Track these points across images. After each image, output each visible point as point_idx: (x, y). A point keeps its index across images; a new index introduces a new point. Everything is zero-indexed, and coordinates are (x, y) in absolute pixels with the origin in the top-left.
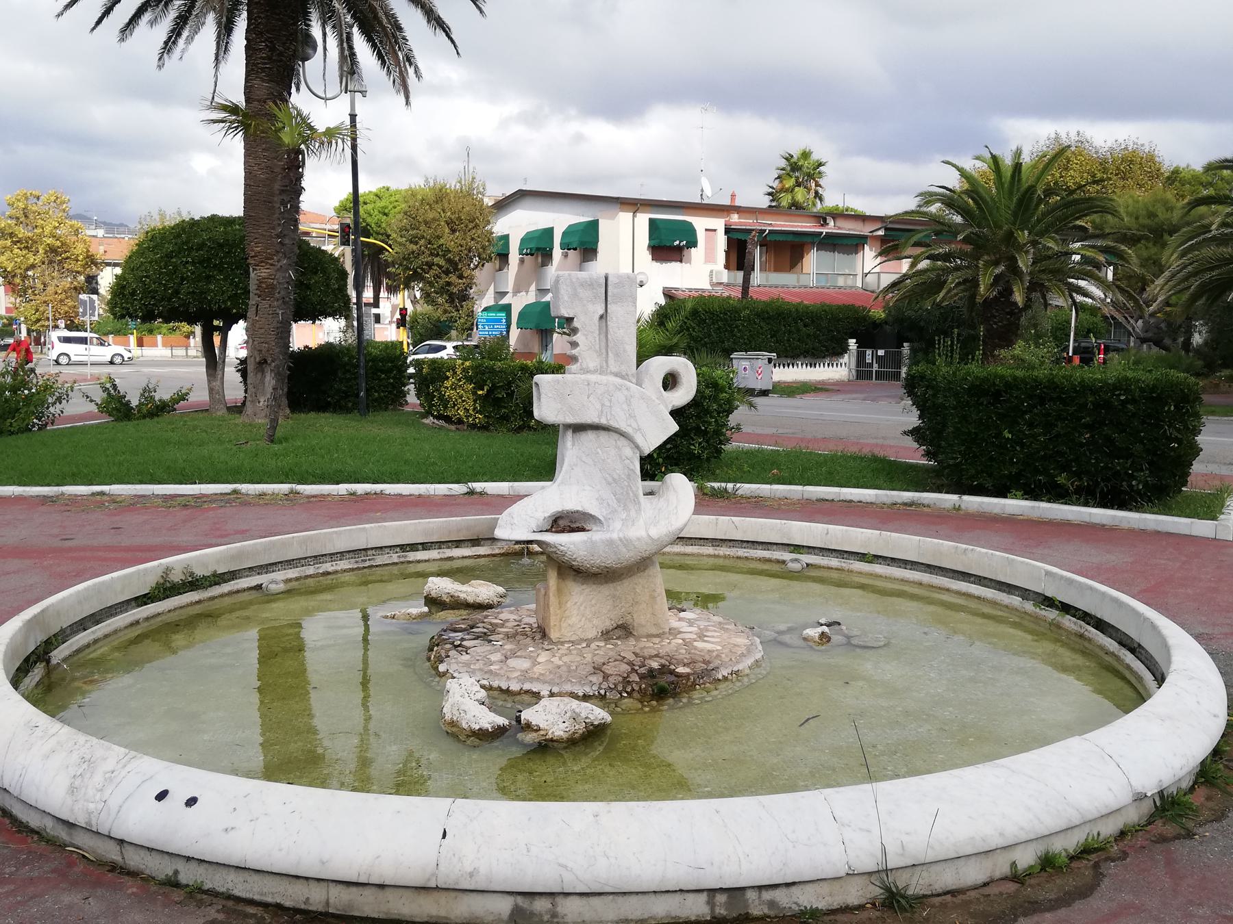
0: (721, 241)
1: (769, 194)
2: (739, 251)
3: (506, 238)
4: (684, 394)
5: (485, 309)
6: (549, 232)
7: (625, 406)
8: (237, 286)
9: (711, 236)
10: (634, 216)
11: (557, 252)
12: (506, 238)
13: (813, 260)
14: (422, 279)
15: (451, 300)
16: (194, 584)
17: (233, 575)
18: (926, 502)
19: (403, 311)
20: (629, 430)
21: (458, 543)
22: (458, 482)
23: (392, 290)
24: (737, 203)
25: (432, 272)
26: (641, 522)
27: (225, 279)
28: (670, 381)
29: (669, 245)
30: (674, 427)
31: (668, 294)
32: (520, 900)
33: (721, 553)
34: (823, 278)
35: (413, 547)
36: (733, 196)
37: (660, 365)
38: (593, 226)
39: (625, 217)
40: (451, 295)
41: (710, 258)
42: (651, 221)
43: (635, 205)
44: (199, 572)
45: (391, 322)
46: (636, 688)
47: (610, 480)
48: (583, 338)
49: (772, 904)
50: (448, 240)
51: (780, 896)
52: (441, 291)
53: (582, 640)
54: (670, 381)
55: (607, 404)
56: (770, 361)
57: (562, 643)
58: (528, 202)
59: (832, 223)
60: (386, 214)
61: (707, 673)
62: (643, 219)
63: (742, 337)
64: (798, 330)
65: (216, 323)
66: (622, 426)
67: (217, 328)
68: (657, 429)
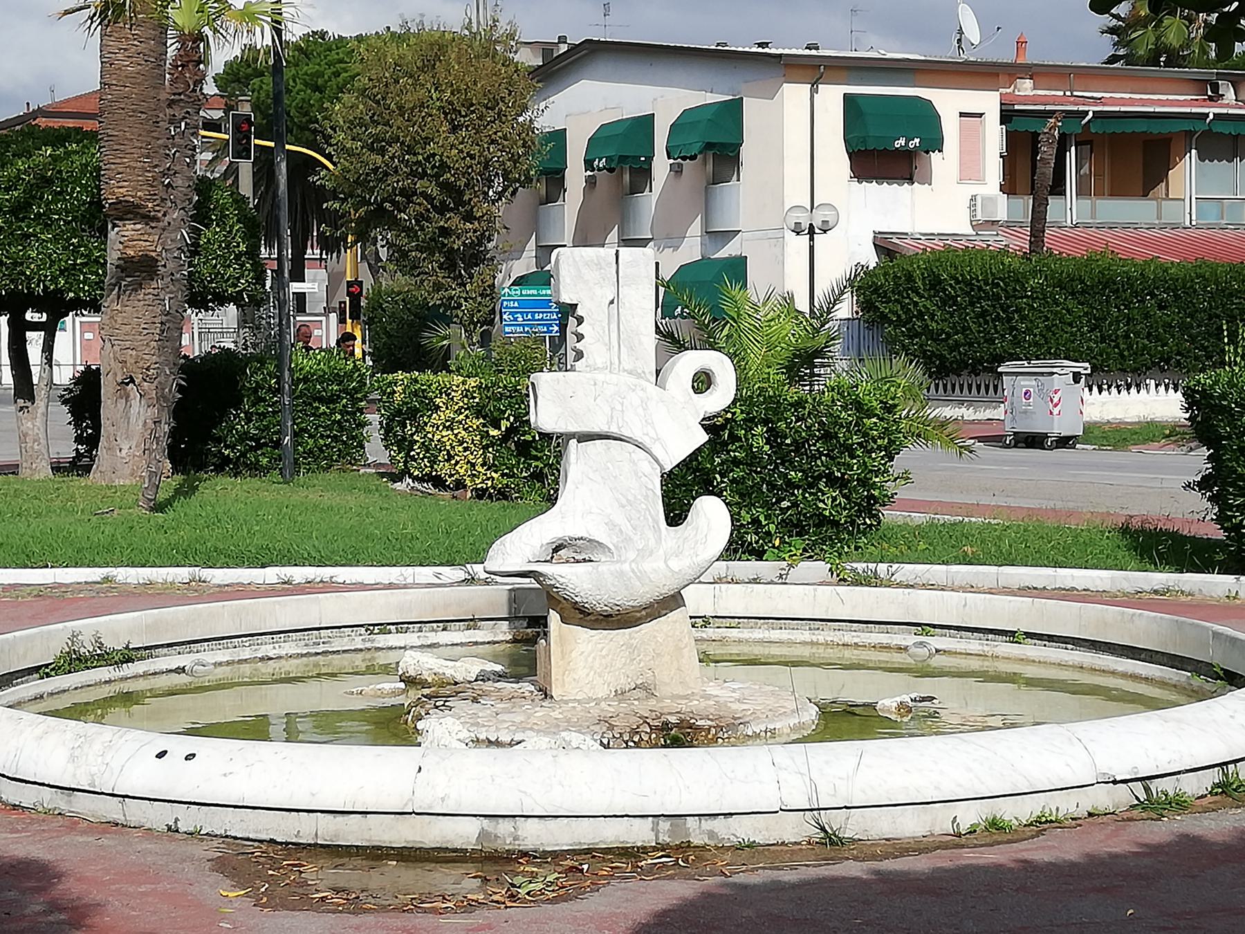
0: (994, 136)
1: (1112, 31)
2: (1030, 159)
3: (559, 137)
4: (720, 397)
5: (519, 282)
6: (647, 123)
7: (640, 410)
8: (75, 251)
9: (970, 125)
10: (814, 91)
11: (661, 166)
12: (559, 137)
13: (1187, 174)
14: (394, 223)
15: (450, 265)
16: (104, 658)
17: (149, 651)
18: (1186, 588)
19: (354, 289)
20: (647, 442)
21: (445, 624)
22: (450, 563)
23: (331, 245)
24: (1030, 58)
25: (411, 209)
26: (661, 552)
27: (55, 240)
28: (703, 382)
29: (886, 149)
30: (703, 437)
31: (884, 246)
32: (486, 821)
33: (821, 639)
34: (1212, 208)
35: (383, 628)
36: (1020, 43)
37: (691, 361)
38: (733, 110)
39: (795, 94)
40: (451, 254)
41: (969, 171)
42: (847, 98)
43: (814, 70)
44: (109, 644)
45: (327, 311)
46: (646, 738)
47: (624, 502)
48: (590, 328)
49: (712, 834)
50: (446, 145)
51: (718, 825)
52: (430, 247)
53: (590, 700)
54: (703, 382)
55: (619, 407)
56: (1077, 377)
57: (566, 702)
58: (603, 65)
59: (1230, 95)
60: (317, 89)
61: (732, 727)
62: (832, 97)
63: (1029, 331)
64: (1147, 316)
65: (30, 316)
66: (638, 436)
67: (35, 327)
68: (682, 439)
